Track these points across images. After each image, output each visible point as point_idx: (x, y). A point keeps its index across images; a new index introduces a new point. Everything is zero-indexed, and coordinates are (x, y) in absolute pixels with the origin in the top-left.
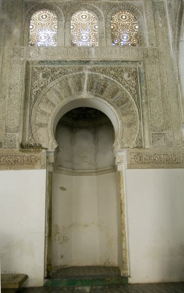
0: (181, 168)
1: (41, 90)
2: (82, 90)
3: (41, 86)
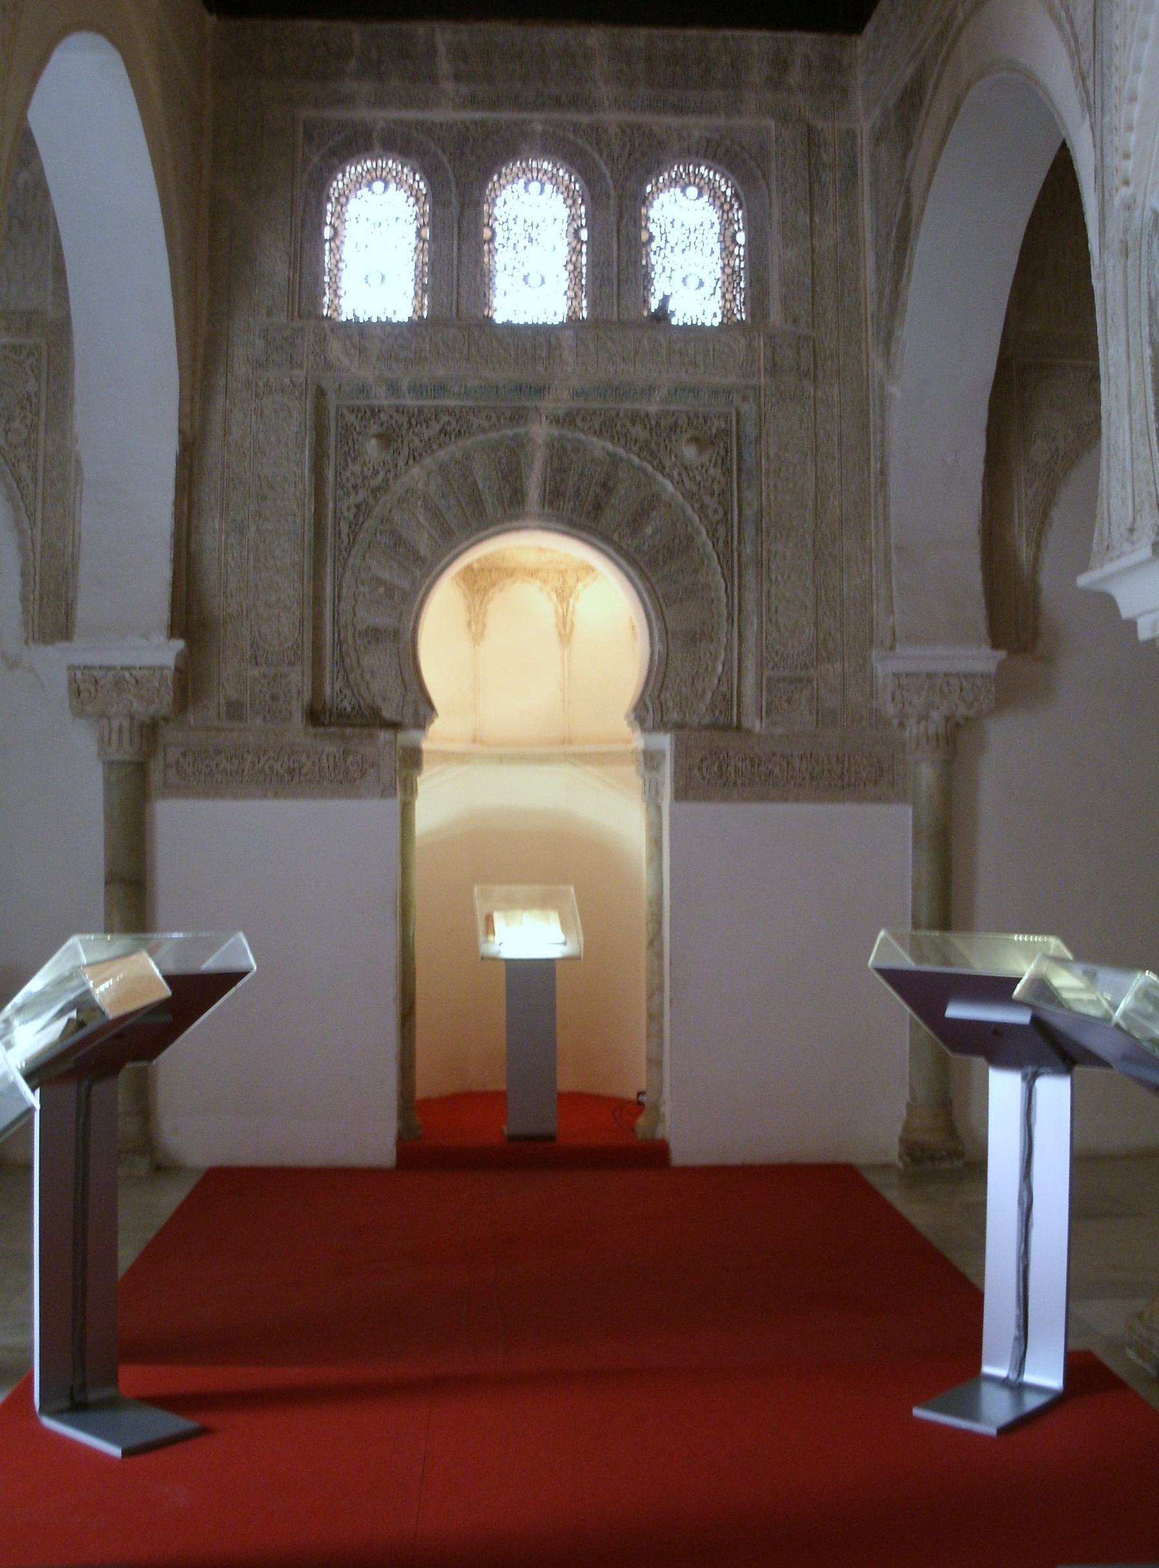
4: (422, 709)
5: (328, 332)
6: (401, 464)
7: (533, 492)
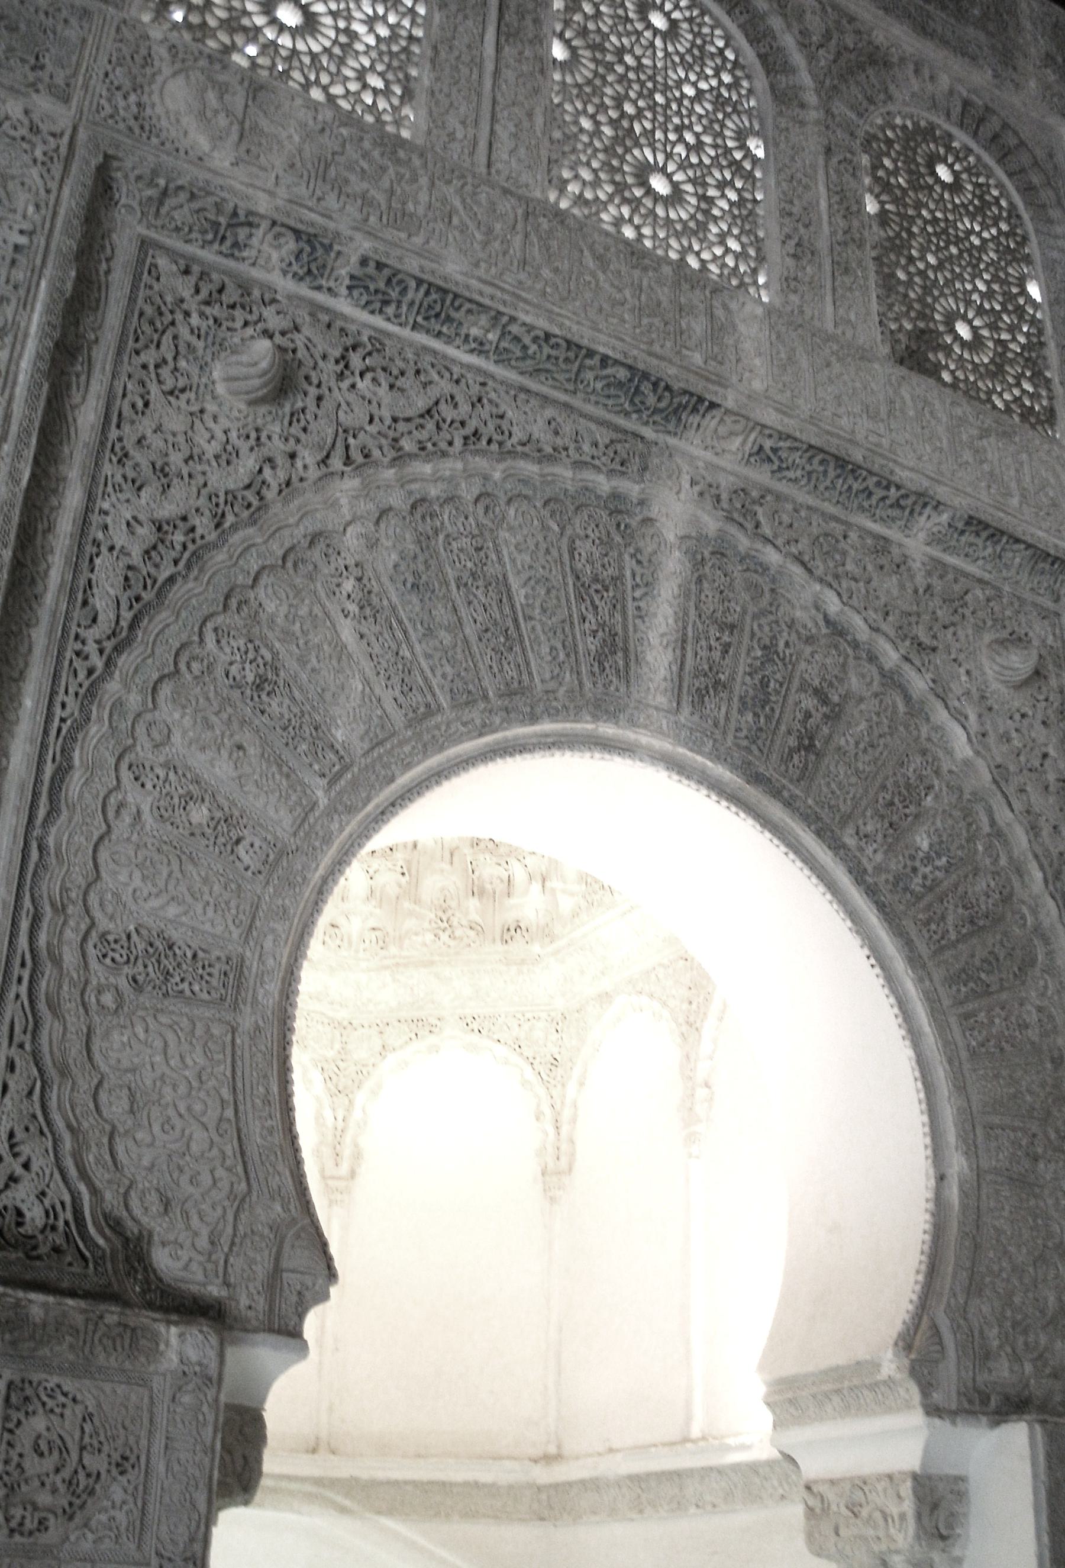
0: (908, 1406)
1: (203, 524)
2: (625, 675)
3: (221, 480)
4: (284, 1269)
5: (161, 51)
6: (308, 457)
7: (658, 659)
